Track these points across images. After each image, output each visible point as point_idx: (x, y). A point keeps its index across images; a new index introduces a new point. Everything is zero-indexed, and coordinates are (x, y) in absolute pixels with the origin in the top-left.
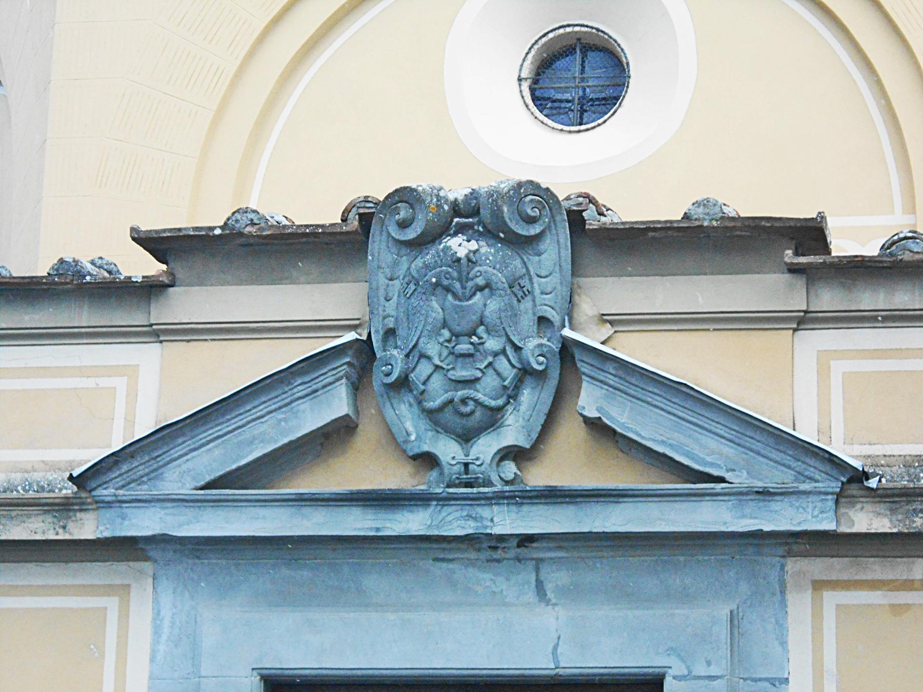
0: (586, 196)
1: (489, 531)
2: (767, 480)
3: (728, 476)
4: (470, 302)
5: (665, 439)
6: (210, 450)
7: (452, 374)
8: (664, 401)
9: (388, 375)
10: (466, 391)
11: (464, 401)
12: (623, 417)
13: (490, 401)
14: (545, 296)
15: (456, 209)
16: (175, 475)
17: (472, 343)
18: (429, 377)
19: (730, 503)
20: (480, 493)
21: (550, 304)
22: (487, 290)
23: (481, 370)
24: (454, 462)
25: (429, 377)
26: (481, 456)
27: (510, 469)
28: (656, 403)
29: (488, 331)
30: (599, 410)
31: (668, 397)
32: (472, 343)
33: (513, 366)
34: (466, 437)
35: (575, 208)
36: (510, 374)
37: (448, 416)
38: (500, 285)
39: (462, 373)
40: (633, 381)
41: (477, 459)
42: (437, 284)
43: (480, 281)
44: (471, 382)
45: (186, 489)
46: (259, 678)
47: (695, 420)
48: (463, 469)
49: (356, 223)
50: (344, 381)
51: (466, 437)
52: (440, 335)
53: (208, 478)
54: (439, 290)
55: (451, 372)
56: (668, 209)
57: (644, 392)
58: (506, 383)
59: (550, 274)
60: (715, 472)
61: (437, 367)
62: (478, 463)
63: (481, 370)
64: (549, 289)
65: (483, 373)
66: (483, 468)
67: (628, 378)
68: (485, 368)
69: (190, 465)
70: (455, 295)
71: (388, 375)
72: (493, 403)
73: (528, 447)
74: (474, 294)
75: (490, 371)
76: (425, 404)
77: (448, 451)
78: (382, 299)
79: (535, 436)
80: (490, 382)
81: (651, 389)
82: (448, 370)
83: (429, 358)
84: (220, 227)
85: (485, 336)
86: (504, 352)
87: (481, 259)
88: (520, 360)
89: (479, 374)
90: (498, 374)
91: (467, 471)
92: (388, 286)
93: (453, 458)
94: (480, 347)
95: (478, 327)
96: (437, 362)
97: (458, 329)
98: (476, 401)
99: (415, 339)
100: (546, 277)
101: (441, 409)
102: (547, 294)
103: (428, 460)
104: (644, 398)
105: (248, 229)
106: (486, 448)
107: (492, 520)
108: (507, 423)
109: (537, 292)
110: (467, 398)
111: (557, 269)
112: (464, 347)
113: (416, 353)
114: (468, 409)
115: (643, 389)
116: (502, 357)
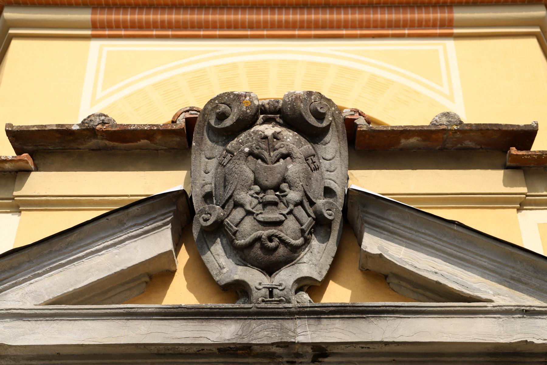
0: (356, 111)
1: (293, 340)
2: (503, 337)
3: (493, 298)
4: (275, 165)
5: (437, 271)
6: (52, 275)
7: (260, 218)
8: (435, 240)
9: (206, 220)
10: (270, 231)
11: (270, 238)
12: (400, 254)
13: (291, 239)
14: (329, 173)
15: (262, 110)
16: (18, 296)
17: (276, 195)
18: (242, 219)
19: (501, 320)
20: (286, 308)
21: (333, 178)
22: (288, 158)
23: (284, 215)
24: (260, 287)
25: (242, 219)
26: (283, 282)
27: (305, 297)
28: (428, 242)
29: (290, 187)
30: (379, 248)
31: (438, 237)
32: (276, 195)
33: (309, 216)
34: (270, 269)
35: (349, 117)
36: (307, 221)
37: (257, 250)
38: (298, 155)
39: (272, 215)
40: (408, 225)
41: (281, 285)
42: (251, 153)
43: (284, 151)
44: (278, 224)
45: (29, 304)
46: (209, 190)
47: (462, 255)
48: (268, 293)
49: (184, 124)
50: (170, 226)
51: (270, 269)
52: (250, 190)
53: (47, 298)
54: (250, 158)
55: (260, 216)
56: (418, 116)
57: (417, 234)
58: (303, 227)
59: (333, 158)
60: (484, 296)
61: (249, 213)
62: (280, 288)
63: (284, 215)
64: (332, 169)
65: (286, 218)
66: (284, 292)
67: (404, 223)
68: (288, 214)
69: (32, 288)
70: (264, 161)
71: (206, 220)
72: (293, 242)
73: (320, 279)
74: (278, 161)
75: (291, 217)
76: (237, 242)
77: (254, 277)
78: (203, 173)
79: (324, 273)
80: (291, 224)
81: (423, 231)
82: (257, 215)
83: (242, 206)
84: (78, 125)
85: (287, 190)
86: (300, 204)
87: (283, 138)
88: (315, 212)
89: (283, 218)
90: (297, 219)
91: (271, 294)
92: (207, 163)
93: (260, 284)
94: (284, 199)
95: (281, 183)
96: (248, 208)
97: (267, 183)
98: (280, 238)
99: (231, 192)
100: (330, 160)
101: (251, 245)
102: (330, 172)
103: (239, 289)
104: (417, 238)
105: (99, 127)
106: (286, 277)
107: (294, 332)
108: (305, 260)
109: (323, 169)
110: (273, 235)
111: (338, 154)
112: (271, 196)
113: (231, 203)
114: (272, 245)
115: (416, 231)
116: (300, 207)
